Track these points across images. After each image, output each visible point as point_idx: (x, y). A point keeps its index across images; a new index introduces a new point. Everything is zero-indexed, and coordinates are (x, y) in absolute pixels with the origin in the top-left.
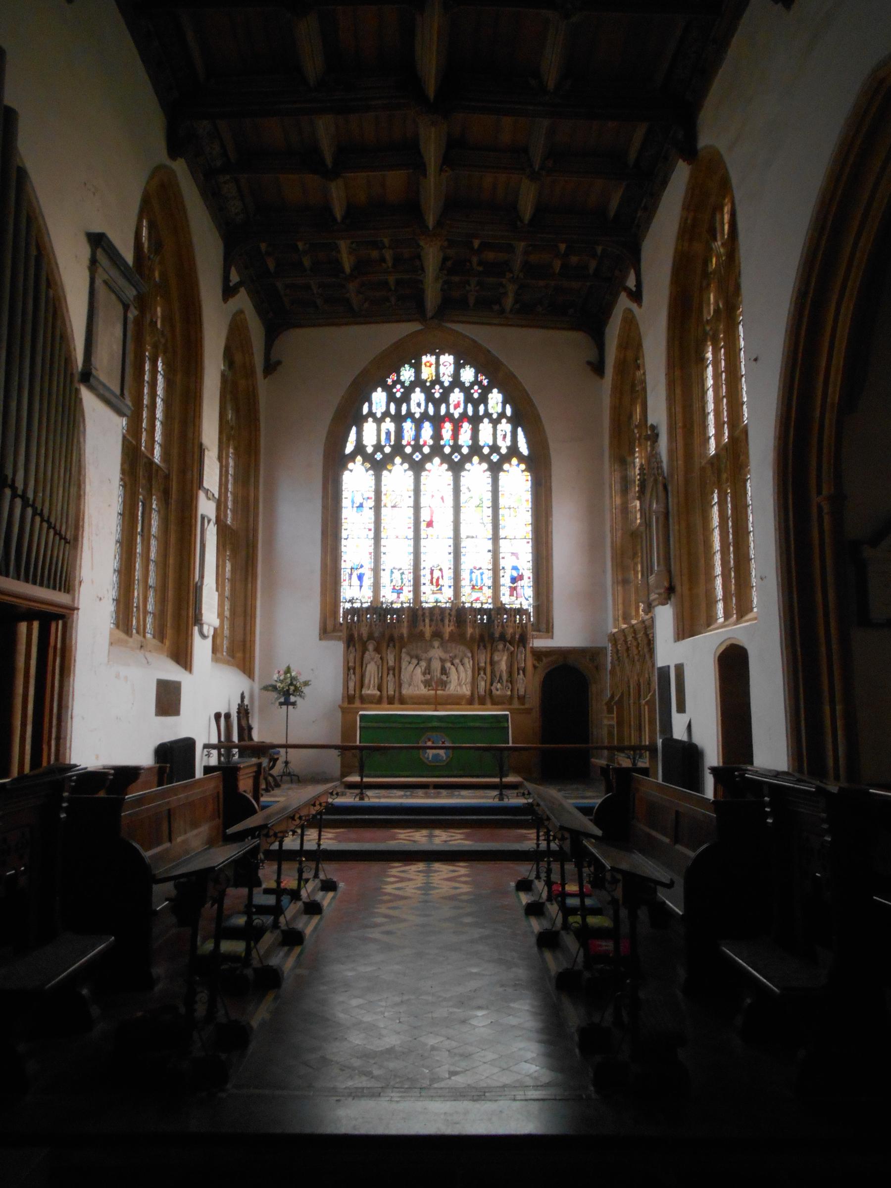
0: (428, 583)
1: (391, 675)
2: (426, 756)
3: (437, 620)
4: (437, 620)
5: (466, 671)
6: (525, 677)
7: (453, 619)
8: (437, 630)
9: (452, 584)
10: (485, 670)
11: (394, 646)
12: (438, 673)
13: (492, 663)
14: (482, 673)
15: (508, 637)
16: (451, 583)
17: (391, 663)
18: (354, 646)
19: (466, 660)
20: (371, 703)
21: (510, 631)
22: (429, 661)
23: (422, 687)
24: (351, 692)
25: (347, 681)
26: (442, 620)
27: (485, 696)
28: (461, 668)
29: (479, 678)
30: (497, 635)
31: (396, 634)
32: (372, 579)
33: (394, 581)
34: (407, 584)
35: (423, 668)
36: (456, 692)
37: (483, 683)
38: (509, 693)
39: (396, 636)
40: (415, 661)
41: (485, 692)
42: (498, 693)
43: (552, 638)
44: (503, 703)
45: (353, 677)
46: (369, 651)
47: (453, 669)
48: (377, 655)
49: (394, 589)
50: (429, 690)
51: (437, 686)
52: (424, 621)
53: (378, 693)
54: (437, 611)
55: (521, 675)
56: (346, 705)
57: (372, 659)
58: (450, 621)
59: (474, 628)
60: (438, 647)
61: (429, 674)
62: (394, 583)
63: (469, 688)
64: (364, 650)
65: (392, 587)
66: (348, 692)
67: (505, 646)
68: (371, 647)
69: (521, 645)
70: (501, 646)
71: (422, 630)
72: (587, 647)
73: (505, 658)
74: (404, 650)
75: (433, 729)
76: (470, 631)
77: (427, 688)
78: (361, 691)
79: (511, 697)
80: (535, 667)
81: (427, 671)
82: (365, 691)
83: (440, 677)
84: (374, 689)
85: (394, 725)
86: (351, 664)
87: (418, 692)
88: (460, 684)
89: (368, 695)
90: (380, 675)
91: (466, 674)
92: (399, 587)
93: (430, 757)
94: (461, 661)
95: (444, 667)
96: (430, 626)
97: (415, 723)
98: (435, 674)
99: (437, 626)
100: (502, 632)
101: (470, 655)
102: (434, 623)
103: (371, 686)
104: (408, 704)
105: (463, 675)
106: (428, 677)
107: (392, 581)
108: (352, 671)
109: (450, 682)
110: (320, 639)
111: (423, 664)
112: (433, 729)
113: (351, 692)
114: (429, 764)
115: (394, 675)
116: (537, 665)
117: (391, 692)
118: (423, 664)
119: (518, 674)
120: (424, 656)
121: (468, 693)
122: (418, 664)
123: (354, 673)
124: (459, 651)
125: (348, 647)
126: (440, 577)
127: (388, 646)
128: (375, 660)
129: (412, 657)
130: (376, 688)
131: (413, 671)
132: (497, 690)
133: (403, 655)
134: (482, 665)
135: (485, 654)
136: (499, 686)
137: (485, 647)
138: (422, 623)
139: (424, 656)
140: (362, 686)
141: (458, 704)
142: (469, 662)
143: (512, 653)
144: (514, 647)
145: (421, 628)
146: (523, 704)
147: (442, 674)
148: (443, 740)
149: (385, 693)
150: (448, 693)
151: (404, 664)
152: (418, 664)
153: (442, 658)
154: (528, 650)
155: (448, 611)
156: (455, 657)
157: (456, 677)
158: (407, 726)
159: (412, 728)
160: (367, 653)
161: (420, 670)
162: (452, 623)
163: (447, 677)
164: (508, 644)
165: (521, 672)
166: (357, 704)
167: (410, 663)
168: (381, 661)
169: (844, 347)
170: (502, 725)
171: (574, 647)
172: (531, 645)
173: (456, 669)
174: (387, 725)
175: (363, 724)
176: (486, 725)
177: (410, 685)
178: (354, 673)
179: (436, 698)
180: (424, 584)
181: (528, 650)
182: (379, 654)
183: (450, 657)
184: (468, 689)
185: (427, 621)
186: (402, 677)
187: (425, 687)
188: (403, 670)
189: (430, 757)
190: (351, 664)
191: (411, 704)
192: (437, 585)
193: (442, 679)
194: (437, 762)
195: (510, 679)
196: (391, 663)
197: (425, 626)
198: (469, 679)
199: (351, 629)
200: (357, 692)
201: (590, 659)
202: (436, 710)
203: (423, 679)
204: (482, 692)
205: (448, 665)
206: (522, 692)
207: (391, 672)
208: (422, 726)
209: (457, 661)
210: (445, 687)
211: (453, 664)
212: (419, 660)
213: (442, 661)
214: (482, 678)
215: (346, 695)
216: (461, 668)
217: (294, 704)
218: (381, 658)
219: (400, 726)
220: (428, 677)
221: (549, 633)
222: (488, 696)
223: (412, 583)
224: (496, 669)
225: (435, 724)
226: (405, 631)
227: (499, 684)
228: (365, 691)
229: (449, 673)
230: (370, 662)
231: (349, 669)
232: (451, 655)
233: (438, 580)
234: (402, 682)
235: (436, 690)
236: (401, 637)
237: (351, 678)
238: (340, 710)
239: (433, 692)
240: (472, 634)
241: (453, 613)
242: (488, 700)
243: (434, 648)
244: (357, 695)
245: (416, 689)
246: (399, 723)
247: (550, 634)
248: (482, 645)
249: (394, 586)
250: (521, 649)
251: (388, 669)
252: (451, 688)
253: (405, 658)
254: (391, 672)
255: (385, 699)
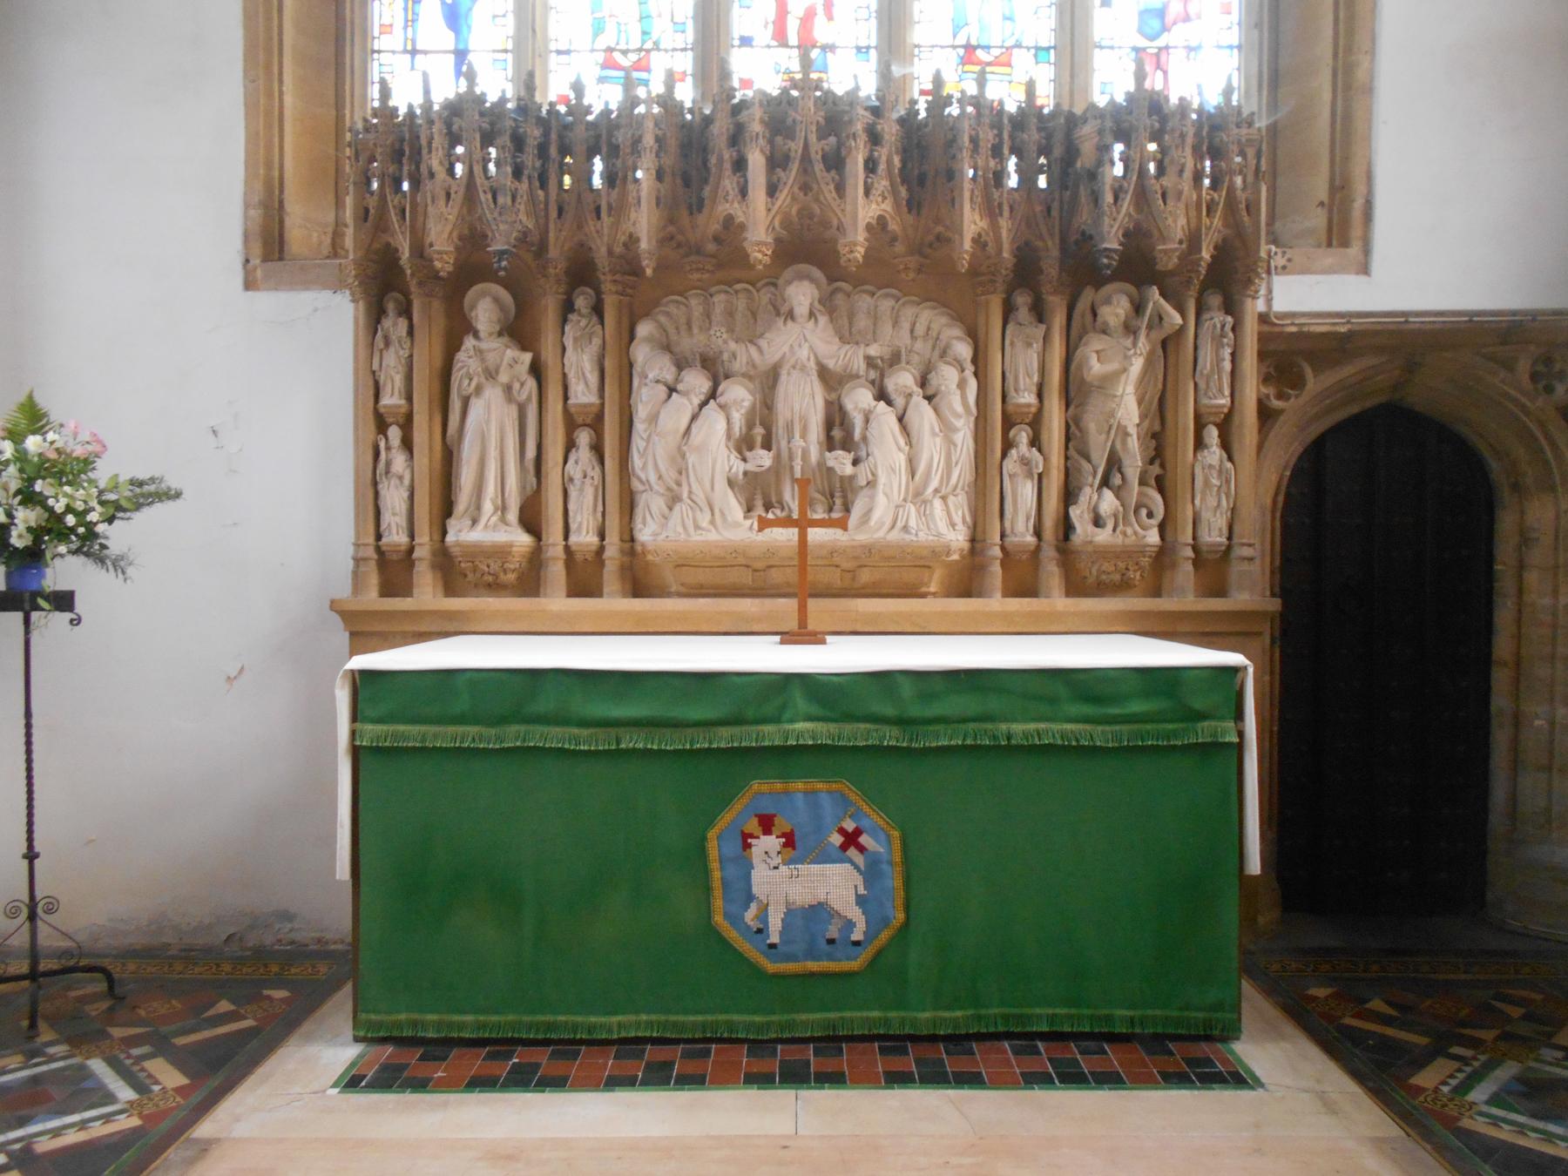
0: (764, 35)
1: (583, 453)
2: (750, 915)
3: (806, 158)
4: (806, 158)
5: (947, 429)
6: (1230, 459)
7: (888, 154)
8: (804, 213)
9: (873, 42)
10: (1036, 423)
11: (598, 310)
12: (808, 443)
13: (1075, 391)
14: (1022, 436)
15: (1168, 252)
16: (868, 33)
17: (583, 394)
18: (406, 311)
19: (947, 377)
20: (495, 587)
21: (1177, 223)
22: (769, 381)
23: (735, 510)
24: (396, 536)
25: (375, 484)
26: (835, 162)
27: (1038, 548)
28: (922, 415)
29: (1010, 465)
30: (1112, 241)
31: (602, 241)
32: (510, 20)
33: (610, 27)
34: (670, 39)
35: (738, 417)
36: (895, 536)
37: (1028, 491)
38: (1153, 537)
39: (601, 255)
40: (697, 382)
41: (1038, 533)
42: (1103, 536)
43: (1364, 269)
44: (1122, 587)
45: (399, 461)
46: (476, 335)
47: (885, 416)
48: (511, 353)
49: (609, 64)
50: (764, 524)
51: (806, 503)
52: (740, 165)
53: (523, 539)
54: (809, 116)
55: (1214, 454)
56: (372, 598)
57: (491, 374)
58: (871, 166)
59: (991, 210)
60: (812, 314)
61: (767, 446)
62: (603, 42)
63: (960, 507)
64: (458, 329)
65: (601, 57)
66: (379, 537)
67: (1138, 308)
68: (485, 310)
69: (1215, 300)
70: (1116, 309)
71: (729, 220)
72: (1534, 315)
73: (1137, 365)
74: (644, 329)
75: (788, 757)
76: (972, 223)
77: (760, 511)
78: (444, 533)
79: (1163, 557)
80: (1266, 415)
81: (759, 431)
82: (461, 533)
83: (821, 464)
84: (503, 520)
85: (554, 737)
86: (391, 400)
87: (713, 536)
88: (917, 496)
89: (477, 552)
90: (531, 453)
91: (950, 443)
92: (633, 57)
93: (775, 923)
94: (923, 383)
95: (841, 409)
96: (772, 190)
97: (677, 724)
98: (798, 442)
99: (805, 188)
100: (1138, 226)
101: (964, 350)
102: (791, 176)
103: (488, 507)
104: (668, 595)
105: (931, 448)
106: (763, 459)
107: (598, 31)
108: (394, 433)
109: (871, 484)
110: (249, 284)
111: (739, 395)
112: (788, 757)
113: (396, 536)
114: (771, 967)
115: (598, 449)
116: (1276, 404)
117: (584, 537)
118: (739, 395)
119: (1199, 444)
120: (741, 355)
121: (958, 538)
122: (713, 395)
123: (407, 444)
124: (913, 337)
125: (376, 315)
126: (820, 10)
127: (568, 308)
128: (504, 378)
129: (681, 365)
130: (513, 516)
131: (689, 428)
132: (1098, 522)
133: (641, 353)
134: (1028, 398)
135: (1037, 346)
136: (1108, 502)
137: (1039, 312)
138: (729, 183)
139: (741, 355)
140: (446, 508)
141: (912, 592)
142: (962, 385)
143: (1168, 345)
144: (1182, 311)
145: (730, 207)
146: (1219, 589)
147: (830, 444)
148: (850, 826)
149: (553, 534)
150: (862, 537)
151: (646, 398)
152: (713, 395)
153: (831, 364)
154: (1251, 328)
155: (861, 120)
156: (895, 359)
157: (901, 460)
158: (633, 741)
159: (661, 753)
160: (469, 342)
161: (721, 426)
162: (881, 184)
163: (855, 462)
164: (1154, 293)
165: (1212, 434)
166: (426, 594)
167: (672, 390)
168: (531, 384)
169: (158, 1161)
170: (1203, 732)
171: (1472, 314)
172: (1260, 306)
173: (901, 419)
174: (513, 735)
175: (371, 732)
176: (1101, 735)
177: (673, 500)
178: (407, 444)
179: (803, 567)
180: (746, 41)
181: (1251, 328)
182: (524, 348)
183: (870, 362)
184: (958, 519)
185: (756, 161)
186: (637, 461)
187: (749, 509)
188: (640, 427)
189: (775, 923)
190: (391, 400)
191: (680, 595)
192: (806, 46)
193: (830, 470)
194: (811, 954)
195: (1155, 470)
196: (583, 394)
197: (743, 192)
198: (963, 470)
199: (382, 226)
200: (424, 539)
201: (1534, 377)
202: (802, 634)
203: (739, 467)
204: (1022, 533)
205: (859, 399)
206: (1214, 535)
207: (584, 438)
208: (724, 738)
209: (903, 380)
210: (847, 509)
211: (882, 395)
212: (716, 371)
213: (831, 380)
214: (1025, 462)
215: (371, 552)
216: (922, 415)
217: (64, 601)
218: (536, 370)
219: (586, 740)
220: (763, 459)
221: (1345, 244)
222: (1049, 553)
223: (690, 36)
224: (1092, 425)
225: (803, 730)
226: (644, 223)
227: (1108, 495)
228: (461, 533)
229: (864, 439)
230: (479, 390)
231: (382, 426)
232: (873, 350)
233: (808, 19)
234: (636, 485)
235: (803, 524)
236: (630, 266)
237: (388, 464)
238: (337, 618)
239: (785, 536)
240: (978, 241)
241: (890, 130)
242: (1052, 573)
243: (791, 315)
244: (423, 552)
245: (704, 521)
246: (584, 723)
247: (1354, 251)
248: (1022, 300)
249: (610, 50)
250: (1218, 319)
251: (571, 425)
252: (877, 515)
253: (650, 363)
254: (584, 438)
255: (556, 571)
